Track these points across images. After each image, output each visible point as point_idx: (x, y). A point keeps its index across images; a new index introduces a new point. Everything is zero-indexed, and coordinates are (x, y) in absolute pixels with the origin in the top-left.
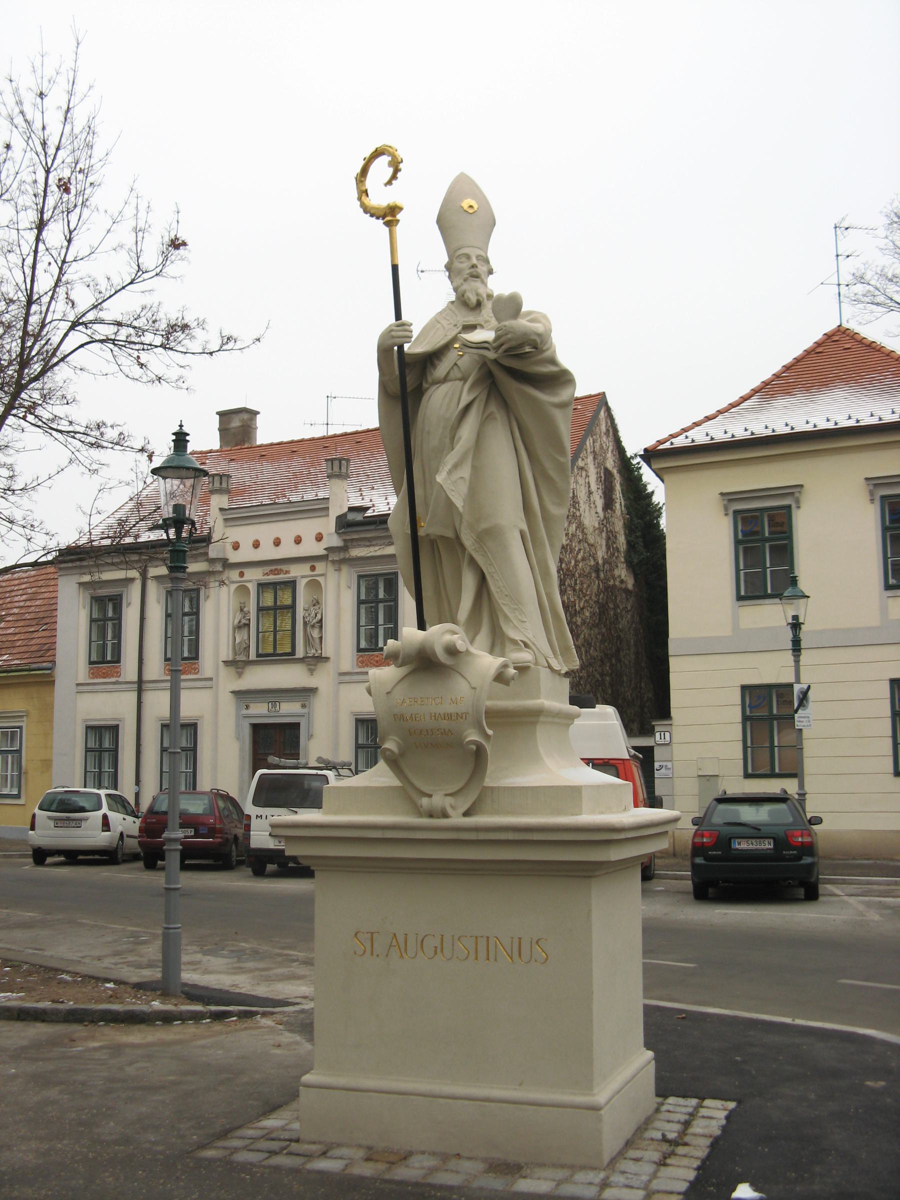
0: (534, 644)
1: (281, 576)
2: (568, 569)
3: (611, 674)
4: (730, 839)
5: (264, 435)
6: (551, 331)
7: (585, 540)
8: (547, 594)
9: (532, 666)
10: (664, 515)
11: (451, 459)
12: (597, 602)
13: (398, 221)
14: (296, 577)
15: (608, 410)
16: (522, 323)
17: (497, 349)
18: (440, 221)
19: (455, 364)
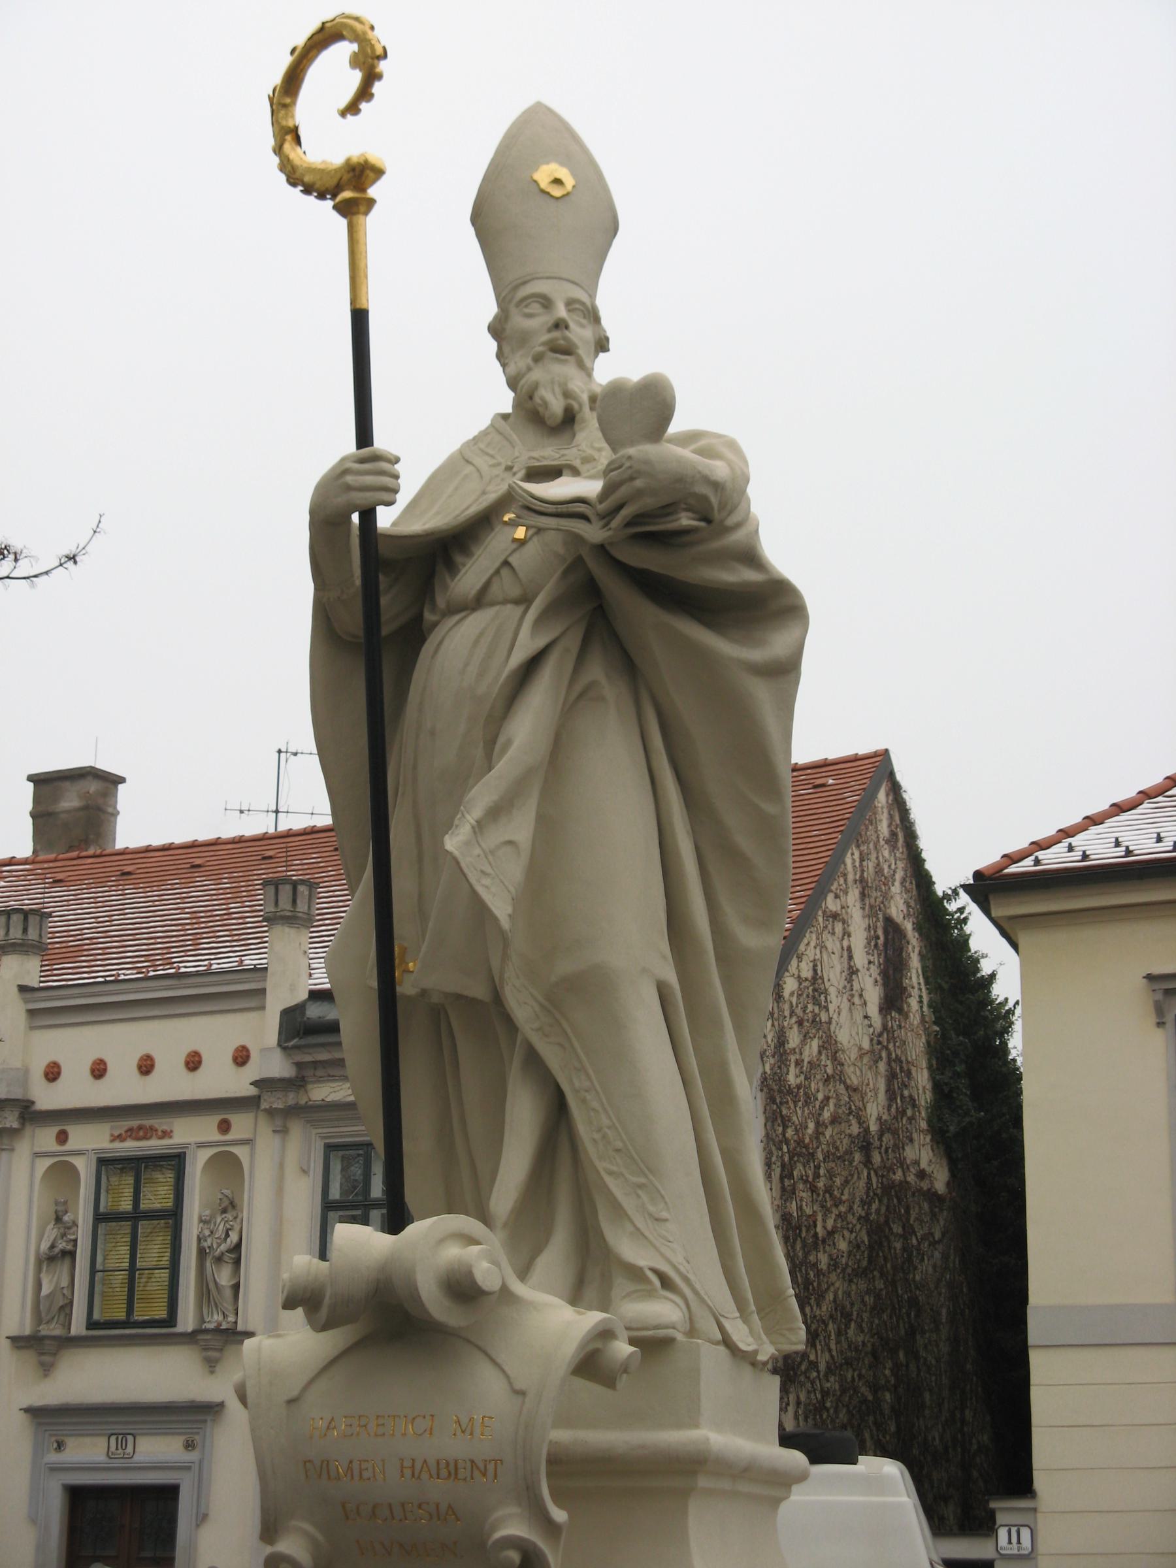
0: (686, 1280)
1: (154, 1142)
2: (800, 1142)
3: (896, 1387)
5: (136, 826)
6: (748, 481)
7: (839, 1077)
8: (724, 1152)
9: (680, 1337)
10: (1018, 1026)
11: (482, 796)
12: (864, 1219)
13: (371, 203)
14: (186, 1146)
15: (896, 789)
16: (669, 453)
18: (480, 218)
19: (506, 563)
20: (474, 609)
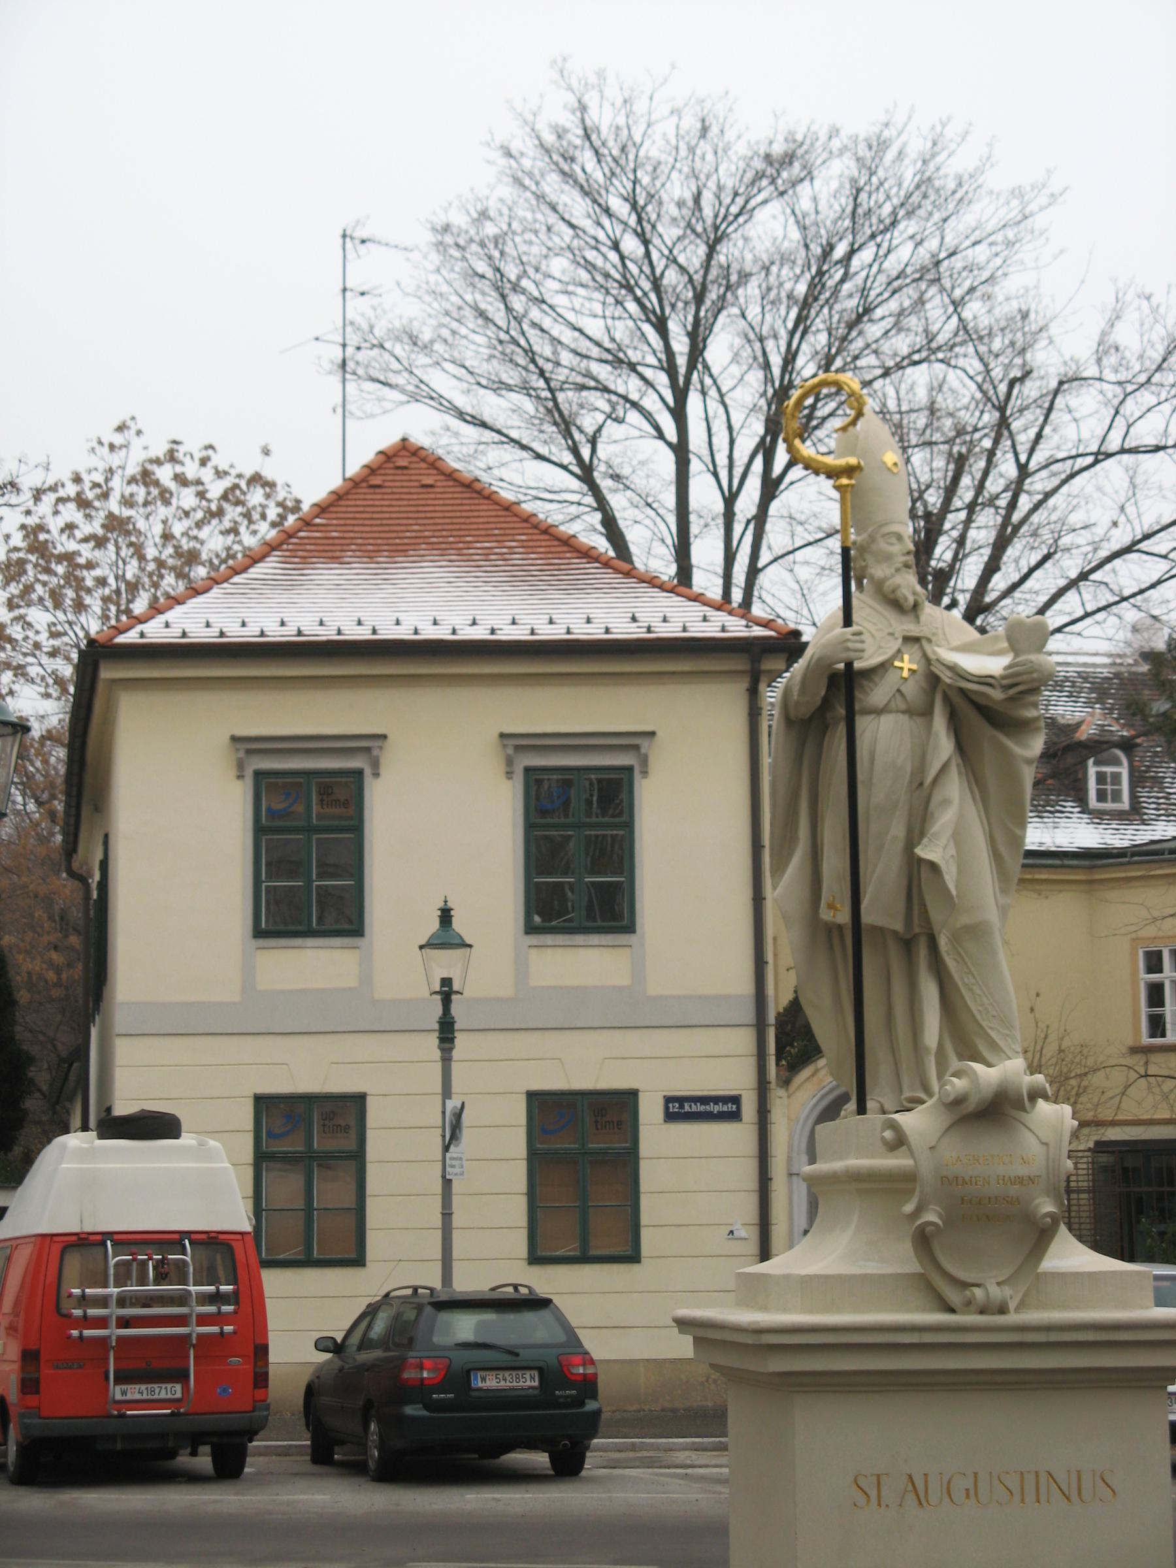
4: (468, 1372)
19: (899, 691)
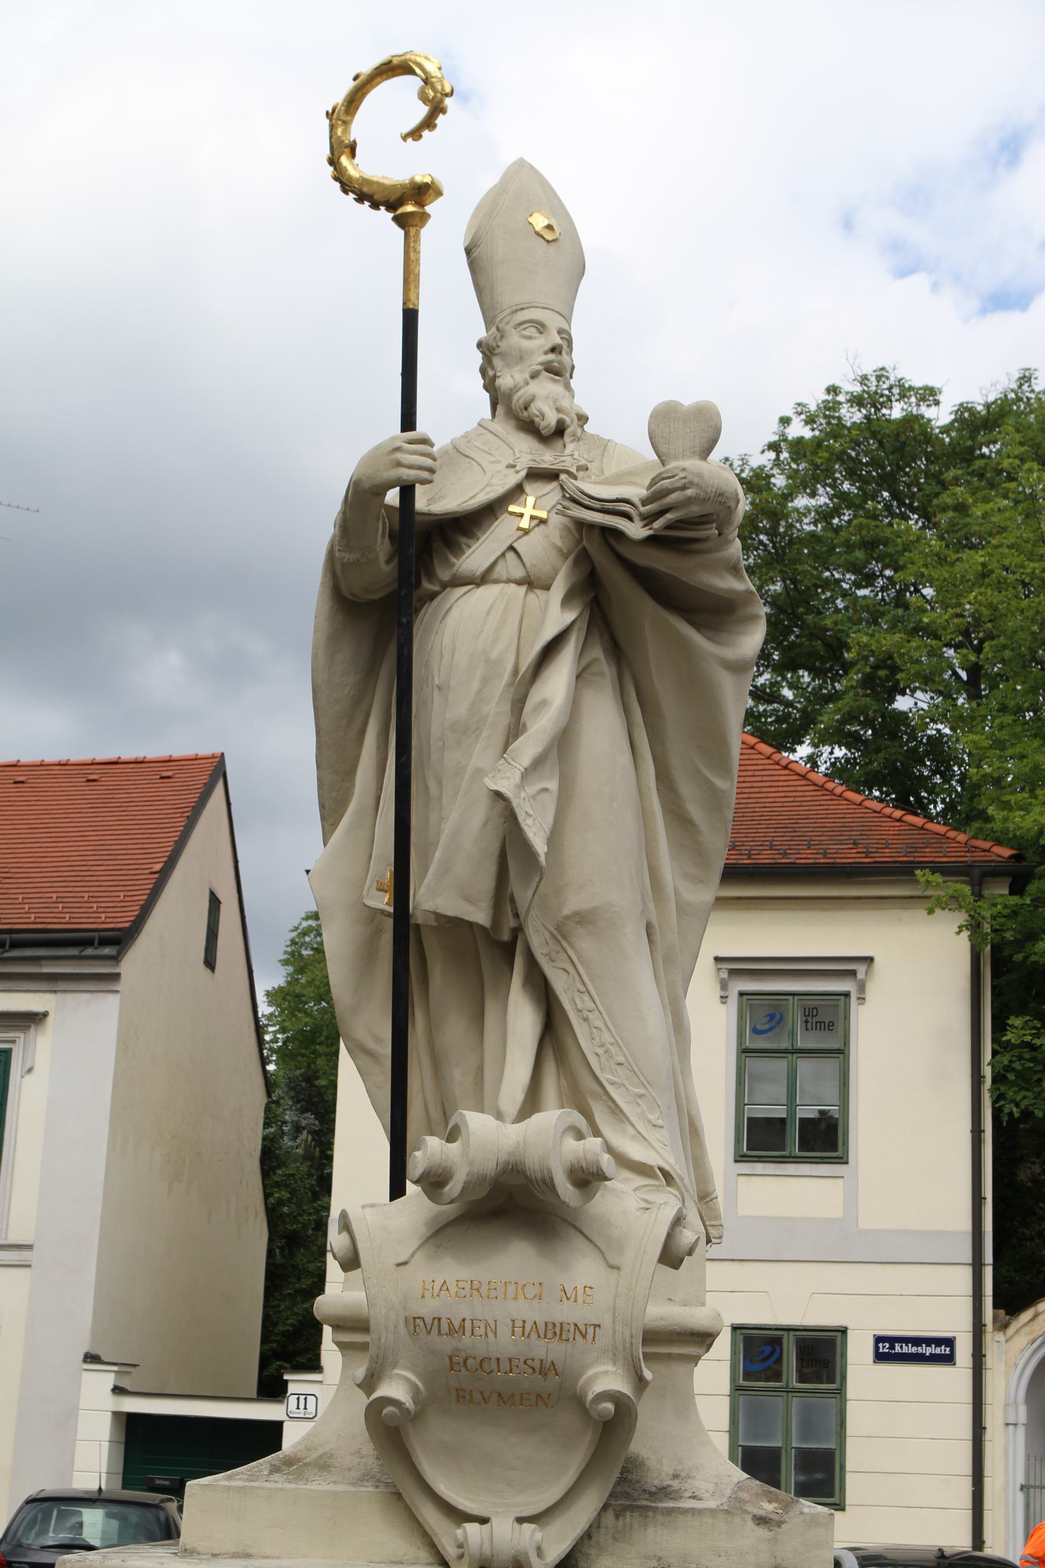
17: (649, 519)
19: (511, 548)
20: (478, 585)
